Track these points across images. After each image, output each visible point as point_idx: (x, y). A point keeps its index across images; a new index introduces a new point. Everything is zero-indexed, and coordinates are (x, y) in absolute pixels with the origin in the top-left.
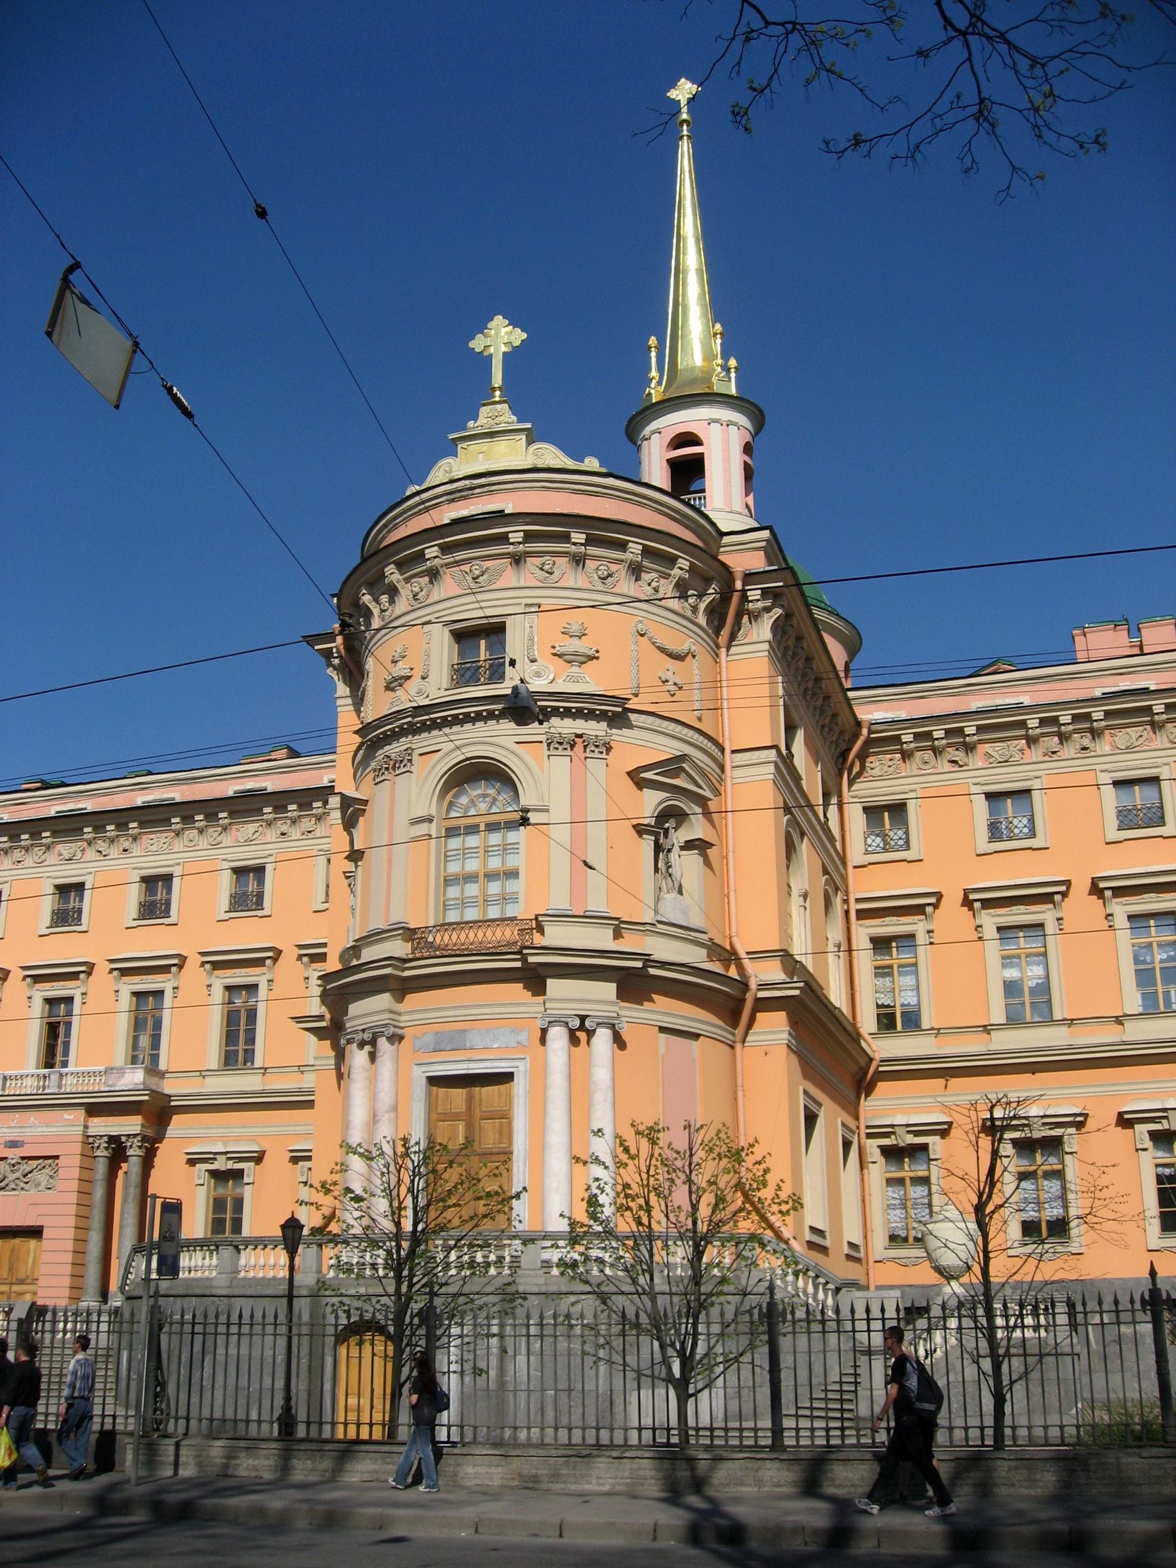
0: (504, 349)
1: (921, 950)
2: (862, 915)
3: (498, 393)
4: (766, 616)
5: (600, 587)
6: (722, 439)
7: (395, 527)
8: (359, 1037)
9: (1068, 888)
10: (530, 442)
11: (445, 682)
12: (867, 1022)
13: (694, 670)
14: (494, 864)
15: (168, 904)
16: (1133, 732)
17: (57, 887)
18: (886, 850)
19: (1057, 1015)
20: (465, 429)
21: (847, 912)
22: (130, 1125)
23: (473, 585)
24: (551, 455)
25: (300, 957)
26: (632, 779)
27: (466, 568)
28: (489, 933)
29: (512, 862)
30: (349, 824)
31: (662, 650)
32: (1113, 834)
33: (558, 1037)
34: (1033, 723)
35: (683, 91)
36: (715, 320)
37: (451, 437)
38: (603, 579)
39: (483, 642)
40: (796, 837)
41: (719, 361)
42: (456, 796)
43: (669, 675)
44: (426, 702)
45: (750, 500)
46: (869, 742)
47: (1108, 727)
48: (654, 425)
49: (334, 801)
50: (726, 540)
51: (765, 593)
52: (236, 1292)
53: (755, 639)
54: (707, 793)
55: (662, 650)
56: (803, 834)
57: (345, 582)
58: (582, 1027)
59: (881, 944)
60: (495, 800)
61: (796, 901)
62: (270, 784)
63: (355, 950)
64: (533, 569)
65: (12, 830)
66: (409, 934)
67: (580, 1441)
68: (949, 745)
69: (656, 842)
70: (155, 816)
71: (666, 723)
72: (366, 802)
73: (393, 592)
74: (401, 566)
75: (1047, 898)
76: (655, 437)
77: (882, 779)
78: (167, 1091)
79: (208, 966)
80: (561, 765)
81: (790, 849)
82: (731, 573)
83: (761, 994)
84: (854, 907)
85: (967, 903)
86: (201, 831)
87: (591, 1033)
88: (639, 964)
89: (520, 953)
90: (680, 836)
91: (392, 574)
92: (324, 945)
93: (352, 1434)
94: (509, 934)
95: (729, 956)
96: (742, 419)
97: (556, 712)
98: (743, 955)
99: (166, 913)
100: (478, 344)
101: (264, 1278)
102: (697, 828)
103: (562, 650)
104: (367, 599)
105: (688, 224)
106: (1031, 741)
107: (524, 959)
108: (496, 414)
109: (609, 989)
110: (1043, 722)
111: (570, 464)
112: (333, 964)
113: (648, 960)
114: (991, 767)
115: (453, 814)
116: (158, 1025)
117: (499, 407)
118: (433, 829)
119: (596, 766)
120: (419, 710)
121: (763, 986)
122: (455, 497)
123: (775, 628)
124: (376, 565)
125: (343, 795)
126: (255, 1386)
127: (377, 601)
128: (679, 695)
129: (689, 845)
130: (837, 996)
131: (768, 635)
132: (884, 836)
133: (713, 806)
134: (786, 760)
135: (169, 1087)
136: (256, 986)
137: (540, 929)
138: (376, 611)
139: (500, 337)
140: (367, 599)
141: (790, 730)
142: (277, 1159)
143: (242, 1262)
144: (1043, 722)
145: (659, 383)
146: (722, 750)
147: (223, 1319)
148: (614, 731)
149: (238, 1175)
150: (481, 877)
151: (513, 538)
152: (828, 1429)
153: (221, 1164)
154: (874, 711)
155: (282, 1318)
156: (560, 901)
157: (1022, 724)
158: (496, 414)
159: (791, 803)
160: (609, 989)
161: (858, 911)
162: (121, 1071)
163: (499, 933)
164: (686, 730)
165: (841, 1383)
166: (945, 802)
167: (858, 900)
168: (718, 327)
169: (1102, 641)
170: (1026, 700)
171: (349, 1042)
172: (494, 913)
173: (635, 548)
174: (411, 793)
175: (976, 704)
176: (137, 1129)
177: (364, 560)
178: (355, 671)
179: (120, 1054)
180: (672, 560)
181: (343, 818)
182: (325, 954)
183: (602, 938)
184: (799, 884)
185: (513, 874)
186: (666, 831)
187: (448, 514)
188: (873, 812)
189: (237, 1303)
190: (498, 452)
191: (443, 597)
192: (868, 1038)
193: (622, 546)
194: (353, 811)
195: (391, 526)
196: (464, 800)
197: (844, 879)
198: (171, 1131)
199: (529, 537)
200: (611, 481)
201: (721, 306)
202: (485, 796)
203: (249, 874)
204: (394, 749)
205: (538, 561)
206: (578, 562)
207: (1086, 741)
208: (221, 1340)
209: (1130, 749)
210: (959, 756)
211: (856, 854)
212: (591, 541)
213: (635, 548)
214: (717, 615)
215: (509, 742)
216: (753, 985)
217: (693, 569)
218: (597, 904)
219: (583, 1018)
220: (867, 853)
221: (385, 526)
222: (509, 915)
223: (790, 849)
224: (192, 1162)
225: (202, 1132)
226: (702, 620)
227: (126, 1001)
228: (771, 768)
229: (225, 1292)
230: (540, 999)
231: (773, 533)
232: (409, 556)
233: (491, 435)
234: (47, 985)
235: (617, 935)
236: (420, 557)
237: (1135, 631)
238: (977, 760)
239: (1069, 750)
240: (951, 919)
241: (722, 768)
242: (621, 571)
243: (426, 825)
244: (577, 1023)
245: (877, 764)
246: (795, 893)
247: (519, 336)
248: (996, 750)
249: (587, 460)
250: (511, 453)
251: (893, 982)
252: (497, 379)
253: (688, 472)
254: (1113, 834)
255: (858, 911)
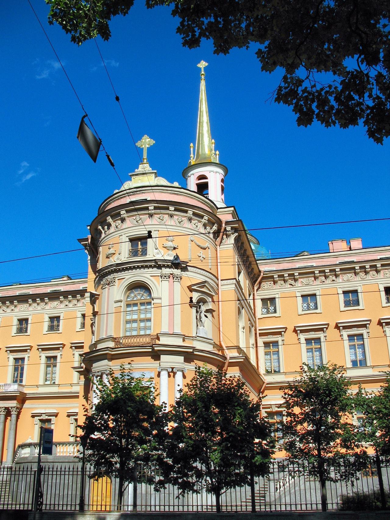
0: (147, 146)
1: (280, 347)
2: (261, 335)
3: (145, 160)
4: (232, 235)
5: (178, 225)
6: (215, 177)
7: (110, 204)
8: (97, 374)
9: (286, 330)
10: (156, 177)
11: (127, 256)
12: (262, 371)
13: (210, 253)
14: (142, 316)
15: (27, 328)
16: (349, 275)
17: (50, 318)
18: (309, 310)
19: (368, 365)
20: (134, 171)
21: (256, 334)
22: (12, 404)
23: (136, 223)
24: (163, 181)
25: (38, 349)
26: (189, 289)
27: (134, 218)
28: (141, 340)
29: (148, 316)
30: (93, 302)
31: (199, 246)
32: (300, 312)
33: (164, 374)
34: (317, 272)
35: (203, 65)
36: (213, 138)
37: (130, 174)
38: (180, 222)
39: (139, 243)
40: (241, 308)
41: (213, 152)
42: (130, 293)
43: (201, 255)
44: (120, 262)
45: (223, 197)
46: (263, 278)
47: (341, 274)
48: (191, 172)
49: (87, 295)
50: (219, 210)
51: (232, 228)
52: (56, 461)
53: (229, 243)
54: (213, 294)
55: (199, 246)
56: (243, 308)
57: (93, 222)
58: (172, 371)
59: (267, 344)
60: (143, 295)
61: (241, 330)
62: (62, 289)
63: (95, 345)
64: (157, 218)
65: (3, 300)
66: (114, 339)
67: (300, 509)
68: (289, 279)
69: (197, 310)
70: (23, 299)
71: (200, 270)
72: (99, 295)
73: (109, 225)
74: (112, 217)
75: (280, 333)
76: (192, 176)
77: (267, 290)
78: (25, 392)
79: (8, 352)
80: (166, 284)
81: (239, 312)
82: (221, 221)
83: (231, 361)
84: (258, 332)
85: (295, 331)
86: (38, 304)
87: (175, 374)
88: (191, 350)
89: (152, 346)
90: (204, 308)
91: (109, 219)
92: (83, 343)
93: (99, 509)
94: (148, 340)
95: (220, 347)
96: (221, 171)
97: (164, 266)
98: (225, 348)
99: (26, 332)
100: (138, 144)
101: (65, 456)
102: (210, 306)
103: (166, 246)
104: (100, 227)
105: (204, 107)
106: (316, 278)
107: (153, 349)
108: (145, 167)
109: (181, 359)
110: (320, 272)
111: (169, 184)
112: (86, 350)
113: (194, 348)
114: (305, 286)
115: (129, 300)
116: (22, 369)
117: (145, 165)
118: (122, 304)
119: (177, 285)
120: (118, 265)
121: (231, 358)
122: (129, 194)
123: (235, 239)
124: (103, 217)
125: (91, 293)
126: (61, 494)
127: (103, 229)
128: (204, 261)
129: (207, 311)
130: (253, 361)
131: (233, 242)
132: (268, 309)
133: (215, 298)
134: (238, 282)
135: (26, 391)
136: (24, 358)
137: (158, 338)
138: (103, 232)
139: (146, 142)
140: (100, 227)
141: (239, 273)
142: (63, 416)
143: (58, 450)
144: (320, 272)
145: (194, 158)
146: (218, 280)
147: (51, 469)
148: (183, 272)
149: (49, 421)
150: (138, 321)
151: (150, 208)
152: (246, 506)
153: (44, 417)
154: (264, 267)
155: (80, 469)
156: (165, 329)
157: (313, 273)
158: (145, 167)
159: (241, 299)
160: (181, 359)
161: (260, 333)
162: (10, 385)
163: (144, 340)
164: (206, 273)
165: (259, 490)
166: (288, 299)
167: (260, 330)
168: (213, 141)
169: (339, 246)
170: (315, 265)
171: (93, 376)
172: (142, 333)
173: (190, 212)
174: (115, 292)
175: (298, 265)
176: (15, 405)
177: (99, 215)
178: (94, 251)
179: (9, 379)
180: (202, 217)
181: (91, 300)
182: (83, 346)
183: (178, 342)
184: (242, 324)
185: (149, 320)
186: (200, 306)
187: (127, 200)
188: (264, 301)
189: (56, 464)
190: (145, 180)
191: (126, 227)
192: (263, 375)
193: (186, 212)
194: (94, 298)
195: (108, 204)
196: (132, 295)
197: (255, 322)
198: (24, 406)
199: (156, 208)
200: (182, 190)
201: (215, 133)
202: (139, 294)
203: (55, 320)
204: (110, 277)
205: (158, 216)
206: (171, 217)
207: (334, 278)
208: (50, 476)
209: (348, 281)
210: (293, 282)
211: (259, 314)
212: (176, 210)
213: (190, 212)
214: (216, 234)
215: (148, 276)
216: (228, 358)
217: (208, 220)
218: (178, 330)
219: (173, 368)
220: (262, 314)
221: (107, 203)
222: (147, 333)
223: (239, 312)
224: (33, 417)
225: (37, 406)
226: (211, 236)
227: (11, 362)
228: (234, 286)
229: (52, 461)
230: (158, 362)
231: (234, 208)
232: (115, 214)
233: (143, 174)
234: (15, 354)
235: (184, 340)
236: (119, 214)
237: (349, 243)
238: (298, 284)
239: (328, 281)
240: (289, 336)
241: (218, 285)
242: (185, 220)
243: (120, 303)
244: (171, 370)
245: (265, 285)
246: (241, 327)
247: (153, 142)
248: (305, 280)
249: (175, 183)
250: (151, 180)
251: (271, 357)
252: (145, 156)
253: (203, 188)
254: (343, 308)
255: (260, 333)
